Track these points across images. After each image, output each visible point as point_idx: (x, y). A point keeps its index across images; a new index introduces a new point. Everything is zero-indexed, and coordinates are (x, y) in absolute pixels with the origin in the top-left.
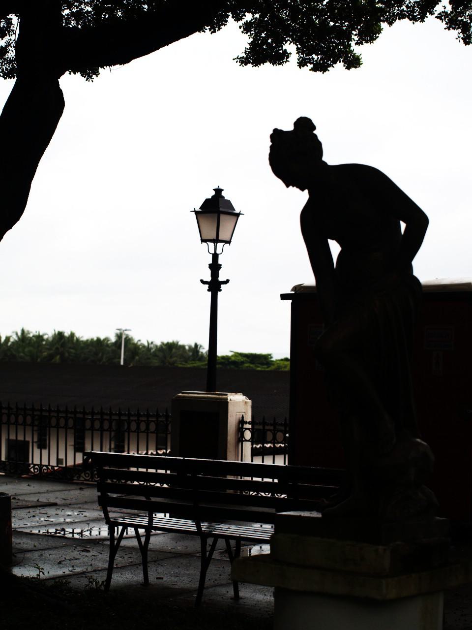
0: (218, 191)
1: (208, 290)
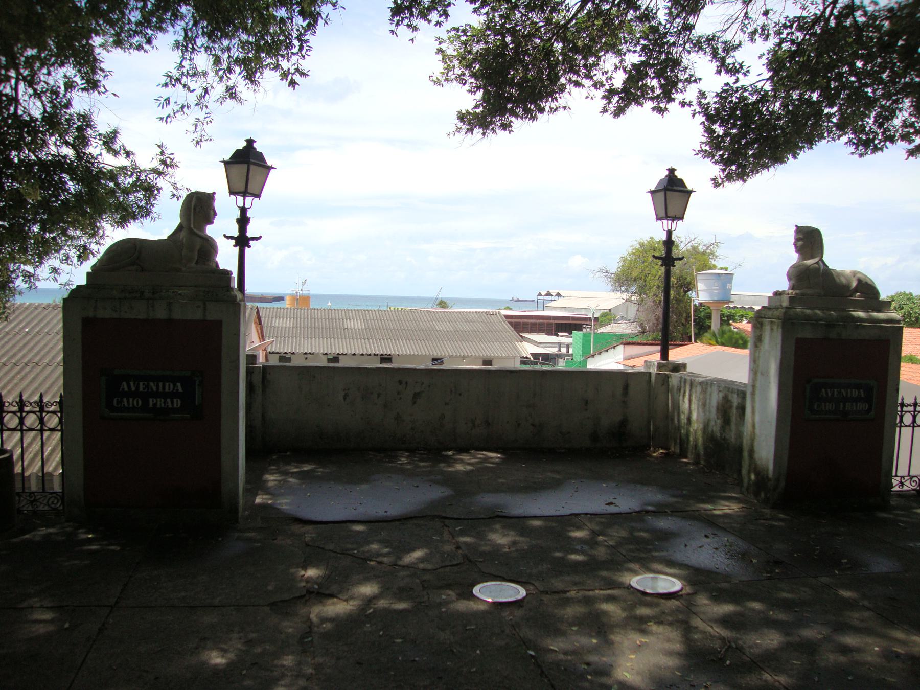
0: (250, 142)
1: (235, 246)
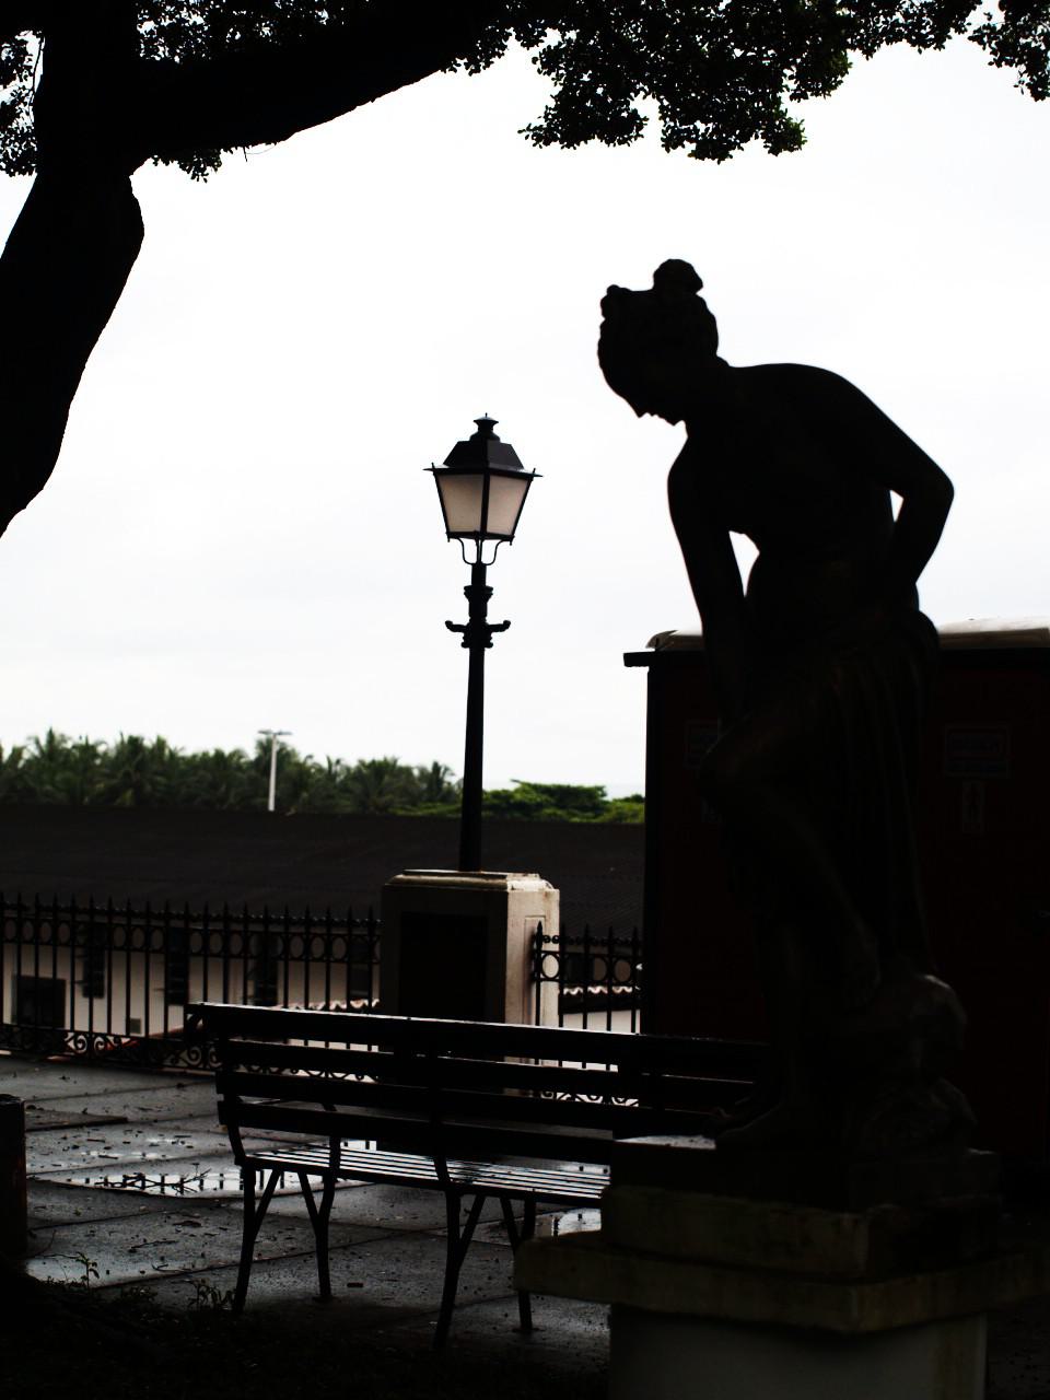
0: (486, 425)
1: (464, 645)
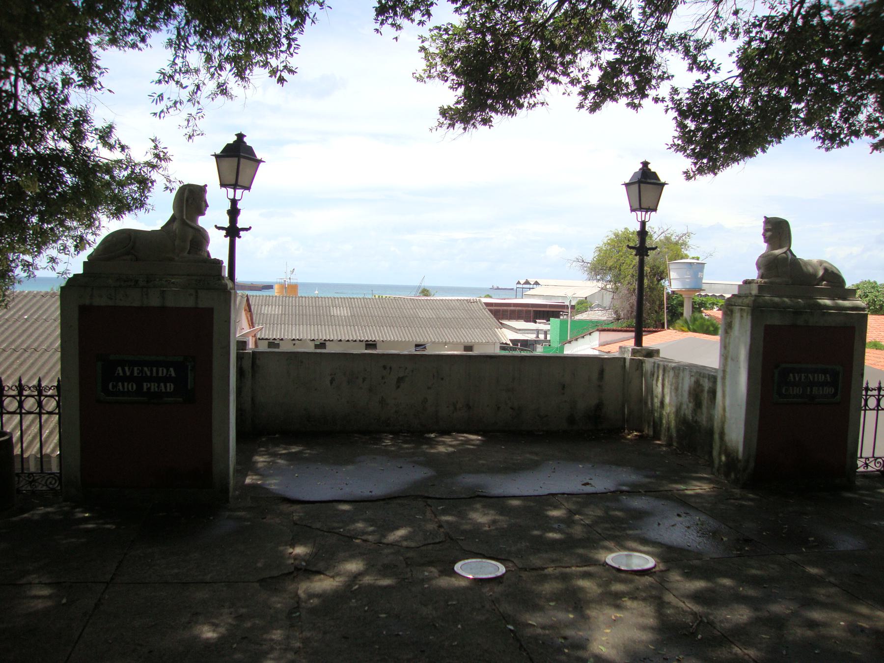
0: (240, 137)
1: (226, 236)
